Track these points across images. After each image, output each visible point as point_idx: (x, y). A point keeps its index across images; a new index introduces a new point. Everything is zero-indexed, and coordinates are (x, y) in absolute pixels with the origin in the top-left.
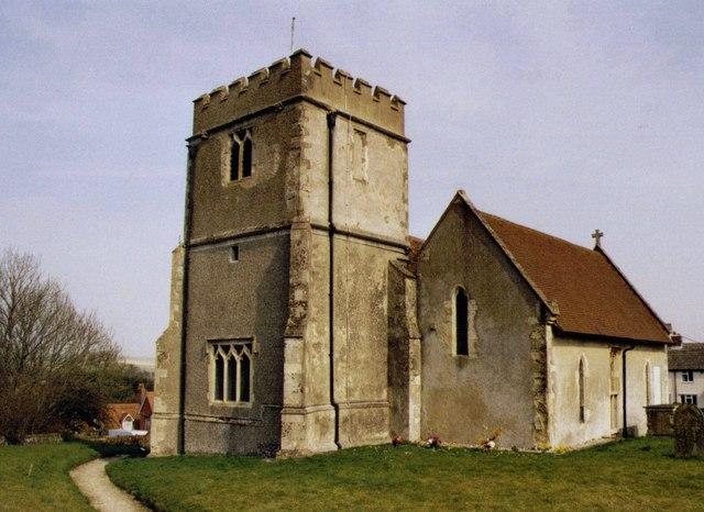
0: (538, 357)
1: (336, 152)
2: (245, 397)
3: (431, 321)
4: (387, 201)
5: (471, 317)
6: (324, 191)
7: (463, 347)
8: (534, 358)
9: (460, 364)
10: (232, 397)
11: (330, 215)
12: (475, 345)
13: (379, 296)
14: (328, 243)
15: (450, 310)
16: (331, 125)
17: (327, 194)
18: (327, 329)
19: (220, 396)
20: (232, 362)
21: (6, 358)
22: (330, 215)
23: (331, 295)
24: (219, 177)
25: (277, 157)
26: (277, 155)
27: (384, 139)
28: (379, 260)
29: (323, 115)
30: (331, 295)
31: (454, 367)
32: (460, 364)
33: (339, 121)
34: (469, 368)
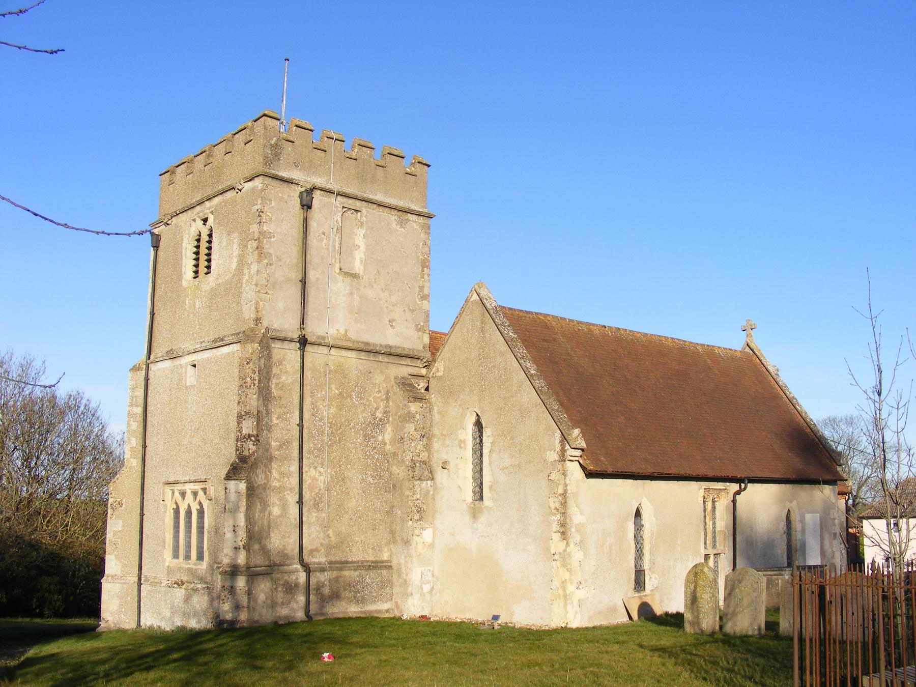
0: (557, 505)
1: (313, 240)
2: (200, 557)
3: (444, 457)
4: (394, 299)
5: (486, 451)
6: (295, 291)
7: (479, 495)
8: (552, 506)
9: (475, 513)
10: (188, 557)
11: (303, 322)
12: (491, 487)
13: (379, 425)
14: (149, 374)
15: (464, 442)
16: (307, 206)
17: (299, 295)
18: (294, 468)
19: (176, 555)
20: (189, 513)
21: (3, 535)
22: (303, 322)
23: (301, 426)
24: (180, 276)
25: (236, 250)
26: (235, 246)
27: (392, 218)
28: (379, 378)
29: (293, 195)
30: (301, 426)
31: (467, 518)
32: (475, 513)
33: (318, 198)
34: (483, 519)
